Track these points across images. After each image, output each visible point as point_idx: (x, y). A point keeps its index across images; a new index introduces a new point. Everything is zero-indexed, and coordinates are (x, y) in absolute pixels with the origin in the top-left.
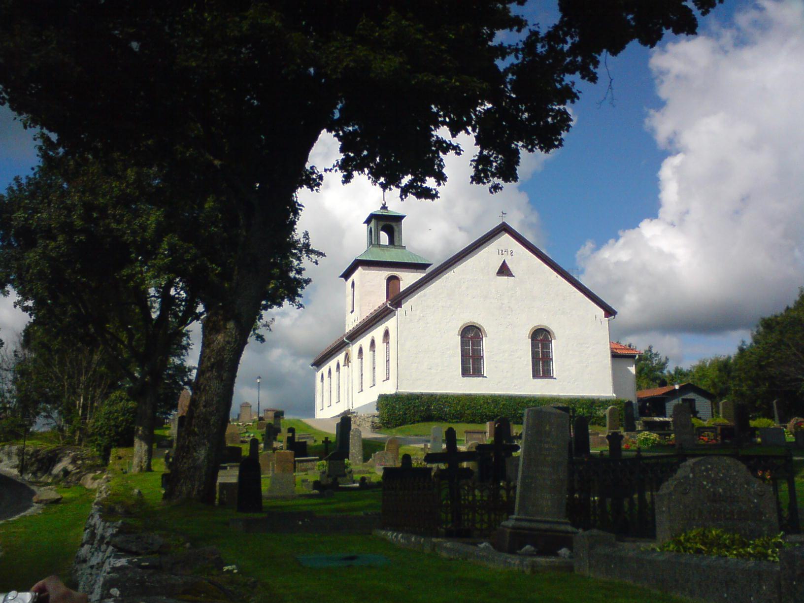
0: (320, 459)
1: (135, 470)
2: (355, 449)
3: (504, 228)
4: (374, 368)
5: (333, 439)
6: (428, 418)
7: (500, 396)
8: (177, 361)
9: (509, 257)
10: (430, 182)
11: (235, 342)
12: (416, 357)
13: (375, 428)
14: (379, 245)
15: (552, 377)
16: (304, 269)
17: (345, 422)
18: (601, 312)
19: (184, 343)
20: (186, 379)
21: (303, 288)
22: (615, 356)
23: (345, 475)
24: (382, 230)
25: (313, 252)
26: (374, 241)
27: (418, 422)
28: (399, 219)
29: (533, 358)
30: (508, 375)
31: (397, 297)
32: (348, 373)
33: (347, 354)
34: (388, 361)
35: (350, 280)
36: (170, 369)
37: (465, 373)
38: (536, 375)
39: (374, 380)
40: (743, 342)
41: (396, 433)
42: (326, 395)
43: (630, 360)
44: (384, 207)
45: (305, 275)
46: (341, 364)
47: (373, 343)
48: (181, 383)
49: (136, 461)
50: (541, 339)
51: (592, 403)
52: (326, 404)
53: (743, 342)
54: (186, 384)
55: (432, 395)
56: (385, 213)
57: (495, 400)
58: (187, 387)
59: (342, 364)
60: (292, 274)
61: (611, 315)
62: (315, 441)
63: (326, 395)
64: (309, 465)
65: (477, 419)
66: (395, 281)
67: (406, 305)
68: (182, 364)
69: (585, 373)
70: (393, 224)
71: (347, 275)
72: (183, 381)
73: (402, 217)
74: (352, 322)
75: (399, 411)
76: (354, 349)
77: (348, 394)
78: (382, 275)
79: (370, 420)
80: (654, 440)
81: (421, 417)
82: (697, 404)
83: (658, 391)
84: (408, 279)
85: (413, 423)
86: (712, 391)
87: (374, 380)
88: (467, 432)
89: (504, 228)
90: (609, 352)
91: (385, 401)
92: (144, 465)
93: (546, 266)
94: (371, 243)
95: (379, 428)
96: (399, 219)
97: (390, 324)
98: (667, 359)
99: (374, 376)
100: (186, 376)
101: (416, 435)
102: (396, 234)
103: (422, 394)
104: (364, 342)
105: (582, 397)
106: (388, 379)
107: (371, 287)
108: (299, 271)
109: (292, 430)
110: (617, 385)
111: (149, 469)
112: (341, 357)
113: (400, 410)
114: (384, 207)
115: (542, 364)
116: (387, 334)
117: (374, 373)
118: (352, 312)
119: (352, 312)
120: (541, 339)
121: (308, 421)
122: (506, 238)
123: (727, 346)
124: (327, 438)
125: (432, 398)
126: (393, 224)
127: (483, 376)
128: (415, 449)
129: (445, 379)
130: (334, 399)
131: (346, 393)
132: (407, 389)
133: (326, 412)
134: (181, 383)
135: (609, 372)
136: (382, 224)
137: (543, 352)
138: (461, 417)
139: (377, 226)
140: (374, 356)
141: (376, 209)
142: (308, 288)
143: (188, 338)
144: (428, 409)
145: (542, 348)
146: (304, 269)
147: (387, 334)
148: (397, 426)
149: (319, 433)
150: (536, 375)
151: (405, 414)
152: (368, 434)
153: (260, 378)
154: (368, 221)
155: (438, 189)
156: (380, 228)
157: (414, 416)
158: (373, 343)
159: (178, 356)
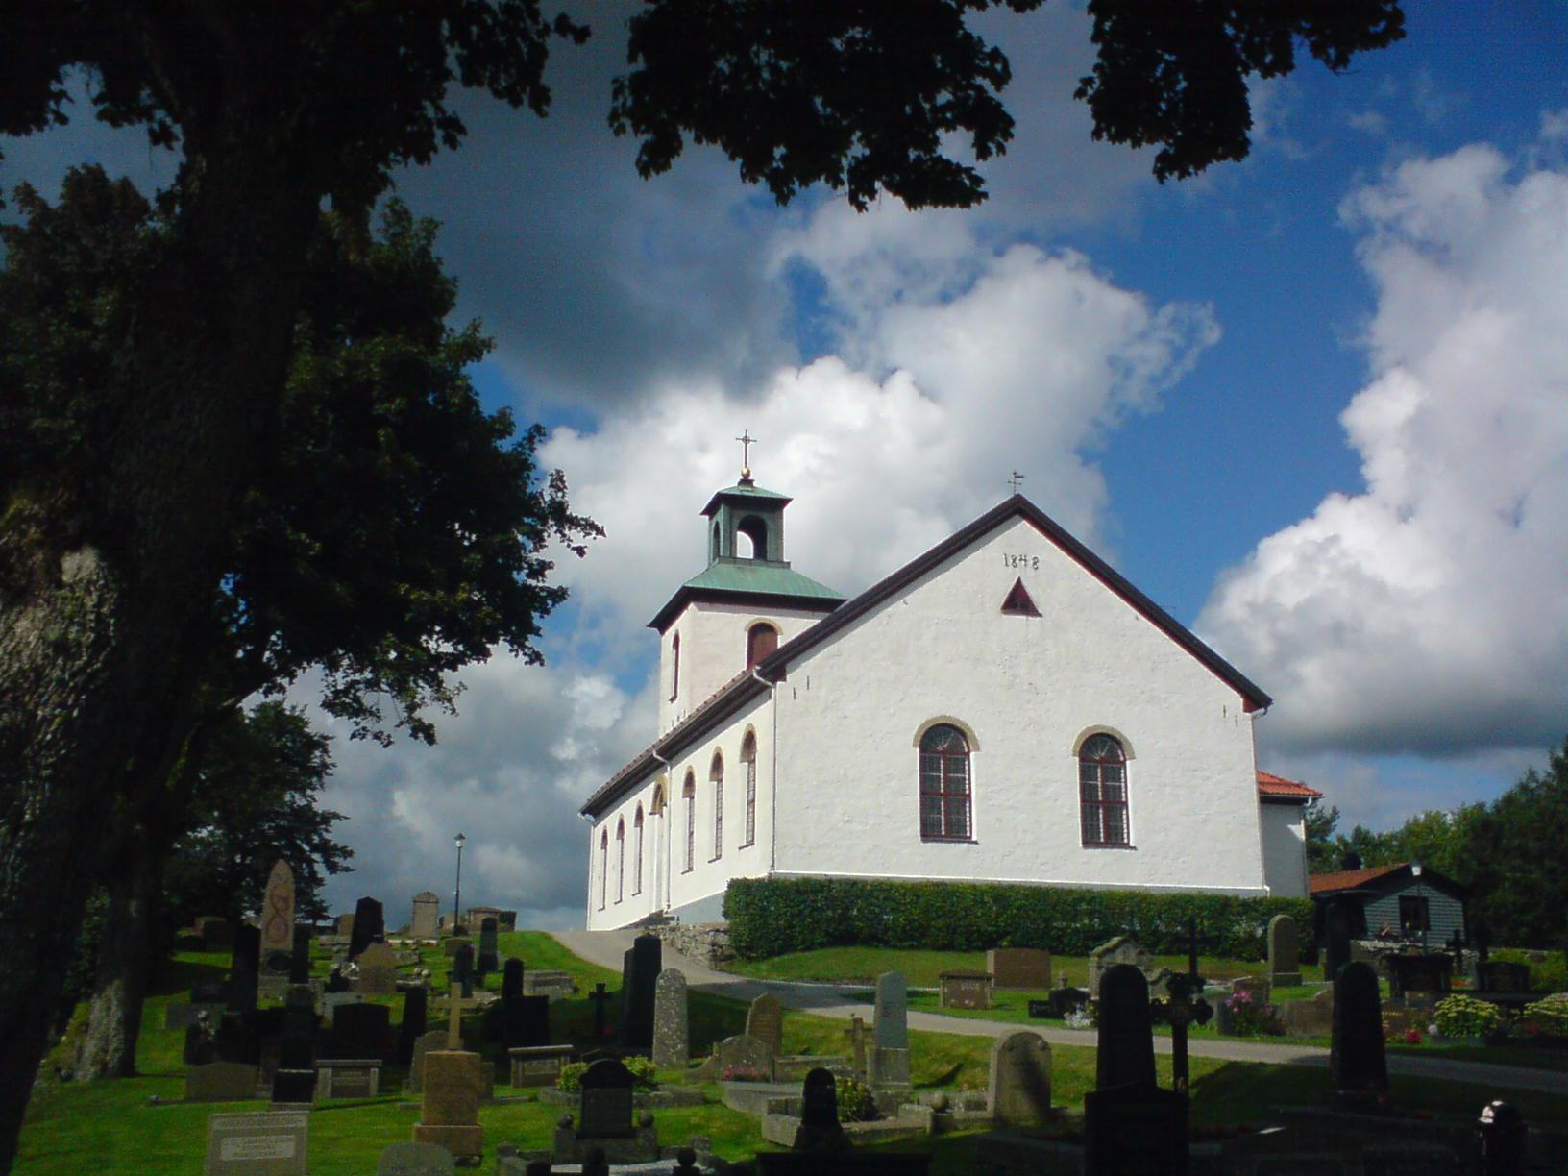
0: (574, 1059)
1: (86, 1073)
2: (668, 1023)
3: (1018, 509)
4: (719, 820)
5: (614, 985)
6: (845, 937)
7: (1011, 887)
8: (301, 802)
9: (1030, 571)
10: (955, 145)
11: (96, 647)
12: (820, 791)
13: (720, 958)
14: (732, 558)
15: (1127, 846)
16: (549, 565)
17: (646, 950)
18: (1236, 700)
19: (316, 761)
20: (316, 839)
21: (545, 611)
22: (1267, 800)
23: (631, 1133)
24: (742, 528)
25: (574, 522)
26: (722, 550)
27: (822, 945)
28: (778, 504)
29: (923, 793)
30: (1024, 838)
31: (771, 663)
32: (661, 829)
33: (659, 788)
34: (751, 803)
35: (670, 633)
36: (283, 816)
37: (929, 832)
38: (1090, 840)
39: (718, 847)
40: (1532, 774)
41: (769, 974)
42: (612, 877)
43: (1294, 810)
44: (746, 481)
45: (551, 580)
46: (647, 809)
47: (717, 763)
48: (306, 848)
49: (91, 1047)
50: (1102, 756)
51: (1223, 907)
52: (611, 896)
53: (1532, 774)
54: (315, 848)
55: (852, 884)
56: (747, 492)
57: (1001, 895)
58: (316, 856)
59: (647, 809)
60: (520, 577)
61: (1259, 707)
62: (576, 990)
63: (612, 877)
64: (546, 1067)
65: (960, 940)
66: (768, 635)
67: (798, 675)
68: (309, 806)
69: (1198, 838)
70: (765, 516)
71: (663, 621)
72: (309, 842)
73: (785, 502)
74: (671, 717)
75: (777, 919)
76: (674, 777)
77: (659, 886)
78: (736, 624)
79: (709, 938)
80: (1489, 1020)
81: (827, 933)
82: (1433, 908)
83: (1347, 881)
84: (791, 627)
85: (808, 949)
86: (1454, 876)
87: (718, 847)
88: (948, 978)
89: (1018, 509)
90: (1254, 789)
91: (748, 899)
92: (113, 1059)
93: (1110, 592)
94: (716, 554)
95: (730, 957)
96: (778, 504)
97: (759, 717)
98: (1335, 812)
99: (718, 838)
100: (316, 831)
101: (817, 980)
102: (770, 537)
103: (830, 881)
104: (698, 759)
105: (1200, 891)
106: (750, 843)
107: (713, 647)
108: (539, 570)
109: (515, 969)
110: (1271, 869)
111: (127, 1067)
112: (645, 795)
113: (787, 919)
114: (746, 481)
115: (1103, 817)
116: (749, 741)
117: (719, 829)
118: (673, 700)
119: (673, 700)
120: (1102, 756)
121: (566, 938)
122: (1023, 528)
123: (1481, 783)
124: (601, 987)
125: (854, 889)
126: (765, 516)
127: (968, 840)
128: (823, 1023)
129: (877, 842)
130: (629, 887)
131: (660, 874)
132: (794, 868)
133: (612, 914)
134: (306, 848)
135: (1255, 834)
136: (742, 514)
137: (1105, 788)
138: (923, 935)
139: (730, 518)
140: (719, 792)
141: (730, 484)
142: (558, 610)
143: (326, 751)
144: (845, 916)
145: (1104, 780)
146: (549, 565)
147: (749, 741)
148: (771, 954)
149: (586, 968)
150: (1090, 840)
151: (791, 927)
152: (699, 973)
153: (461, 837)
154: (711, 510)
155: (981, 168)
156: (736, 522)
157: (812, 932)
158: (717, 763)
159: (302, 790)
